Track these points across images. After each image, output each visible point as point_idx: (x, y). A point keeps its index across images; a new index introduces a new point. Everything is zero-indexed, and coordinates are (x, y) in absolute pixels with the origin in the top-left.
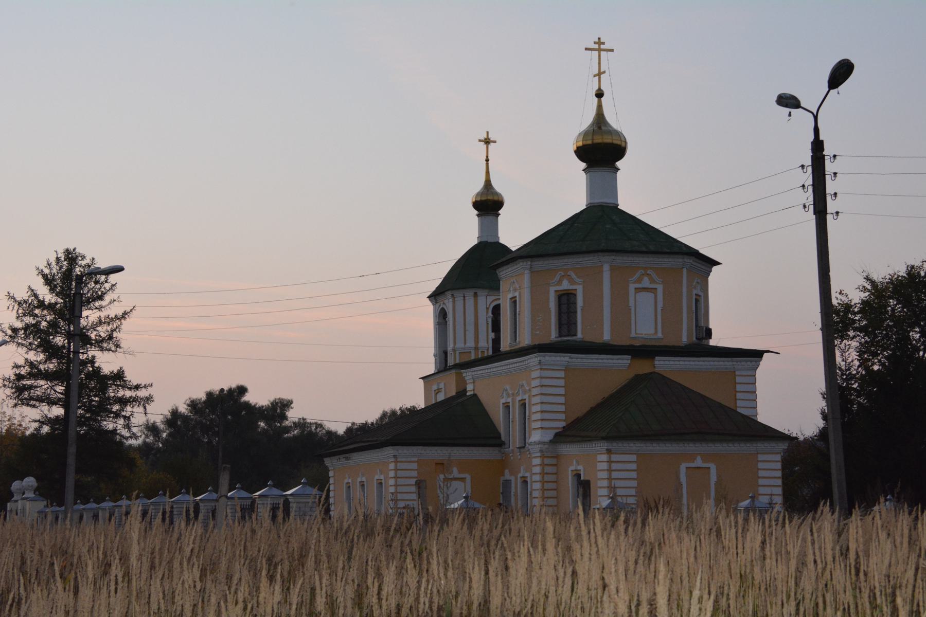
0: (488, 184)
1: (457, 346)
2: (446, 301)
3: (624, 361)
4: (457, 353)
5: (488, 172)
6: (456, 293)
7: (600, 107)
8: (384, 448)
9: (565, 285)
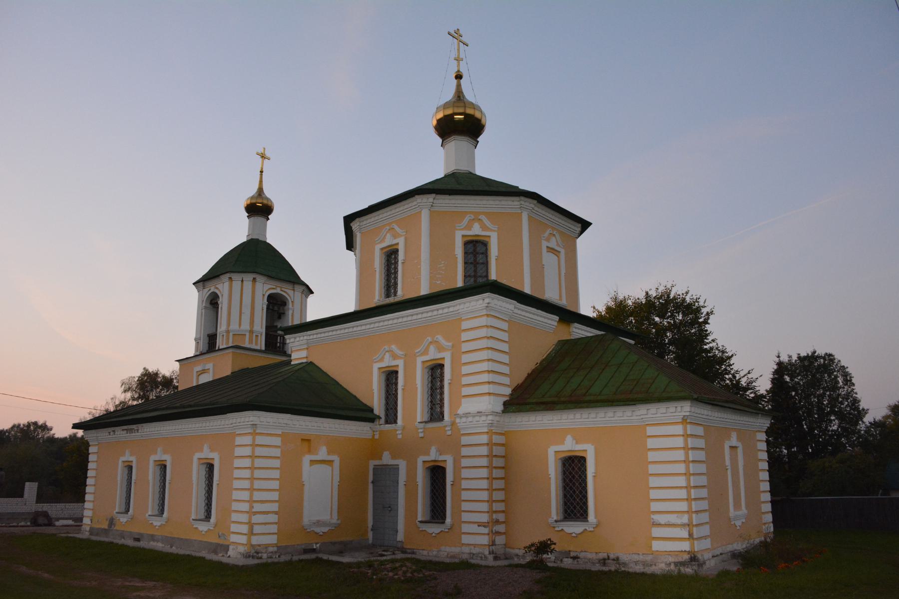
0: (260, 191)
1: (231, 328)
2: (220, 286)
3: (552, 320)
4: (231, 334)
5: (261, 182)
6: (235, 276)
7: (459, 86)
8: (229, 415)
9: (476, 230)
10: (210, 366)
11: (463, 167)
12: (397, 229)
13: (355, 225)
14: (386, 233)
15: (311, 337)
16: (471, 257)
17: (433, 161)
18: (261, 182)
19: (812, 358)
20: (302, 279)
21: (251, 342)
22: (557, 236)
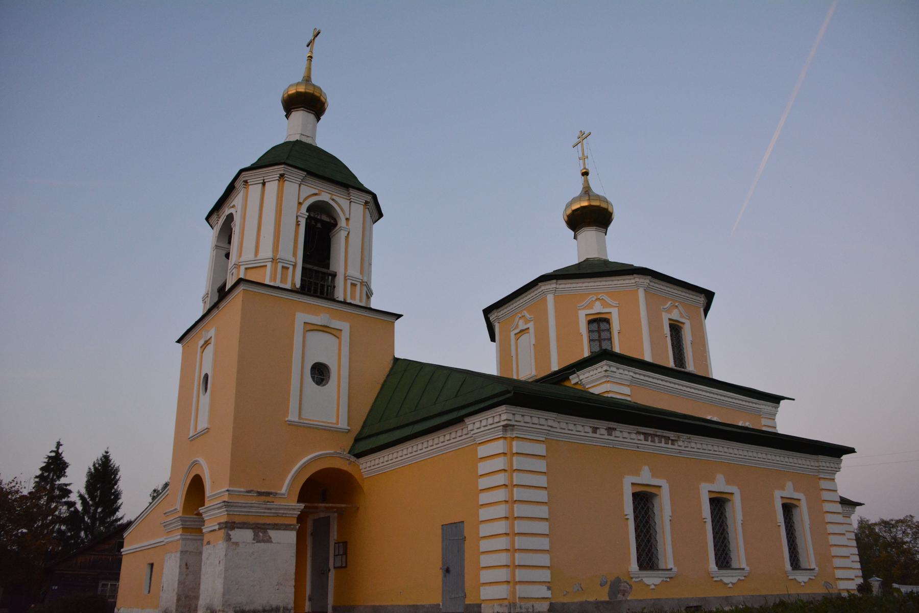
4: (349, 282)
5: (309, 69)
7: (586, 181)
9: (598, 308)
10: (212, 333)
11: (593, 254)
12: (528, 316)
13: (492, 317)
14: (519, 317)
15: (637, 376)
16: (604, 335)
17: (568, 250)
18: (309, 69)
21: (274, 278)
22: (680, 307)
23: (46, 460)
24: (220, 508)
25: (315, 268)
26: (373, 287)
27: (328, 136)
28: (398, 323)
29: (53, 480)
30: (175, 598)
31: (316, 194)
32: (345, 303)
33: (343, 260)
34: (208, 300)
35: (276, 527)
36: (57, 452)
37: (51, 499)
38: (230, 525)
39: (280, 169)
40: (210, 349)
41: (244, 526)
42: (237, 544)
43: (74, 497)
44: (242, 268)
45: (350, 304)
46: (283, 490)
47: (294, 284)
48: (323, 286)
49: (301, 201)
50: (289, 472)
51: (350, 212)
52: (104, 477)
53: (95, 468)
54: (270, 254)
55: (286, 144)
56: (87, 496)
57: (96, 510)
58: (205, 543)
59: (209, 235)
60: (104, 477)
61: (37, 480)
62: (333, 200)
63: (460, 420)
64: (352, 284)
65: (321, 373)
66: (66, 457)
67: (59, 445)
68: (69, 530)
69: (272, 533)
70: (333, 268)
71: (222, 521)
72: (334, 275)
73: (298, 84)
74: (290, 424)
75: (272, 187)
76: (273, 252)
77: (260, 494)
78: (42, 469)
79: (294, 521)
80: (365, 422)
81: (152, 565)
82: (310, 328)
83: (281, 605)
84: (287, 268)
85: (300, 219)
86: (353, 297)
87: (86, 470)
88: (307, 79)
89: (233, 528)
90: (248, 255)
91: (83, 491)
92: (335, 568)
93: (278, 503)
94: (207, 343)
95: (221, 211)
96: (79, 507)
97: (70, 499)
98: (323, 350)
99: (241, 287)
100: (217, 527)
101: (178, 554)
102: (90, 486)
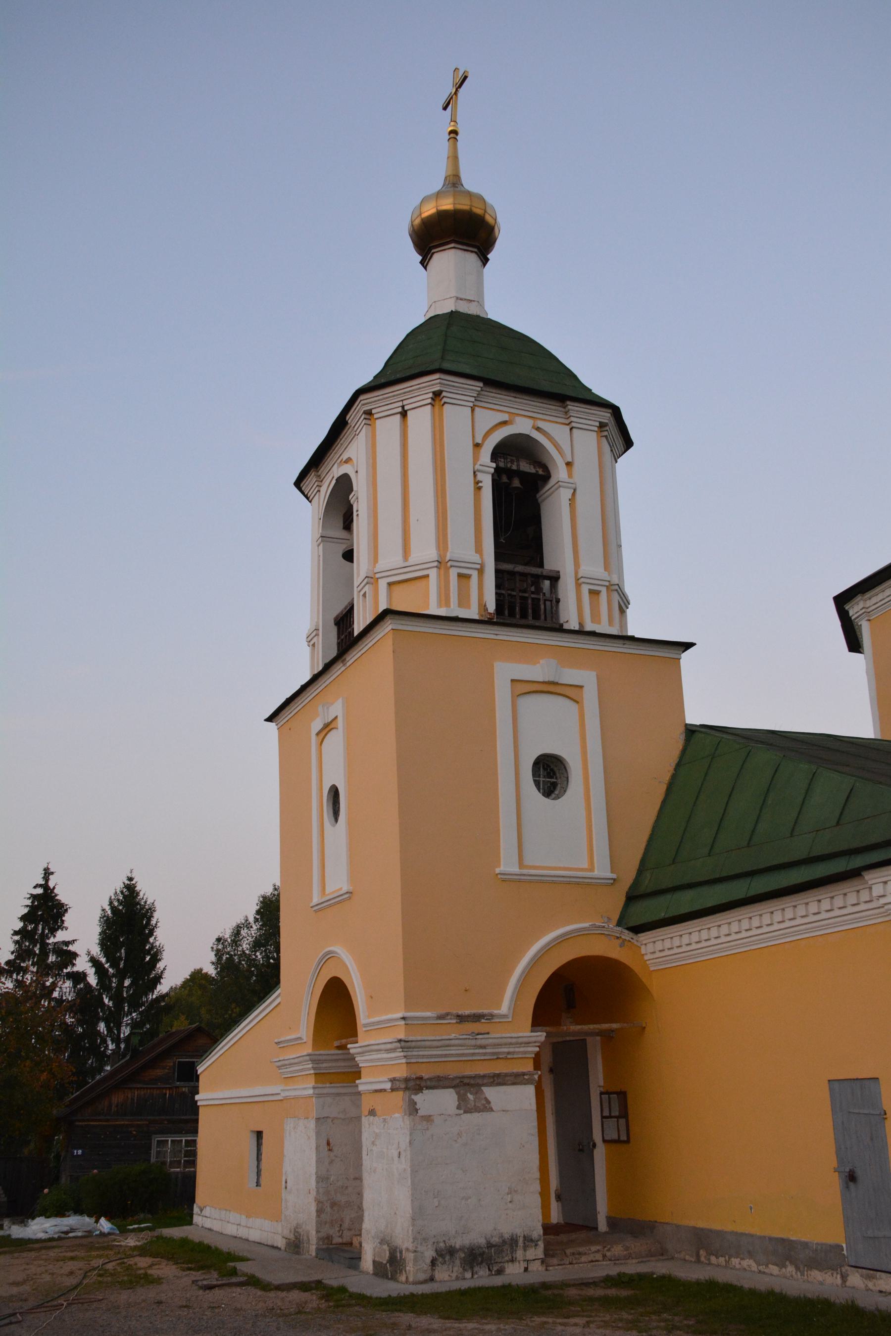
1: (383, 564)
4: (585, 589)
5: (454, 158)
10: (337, 709)
13: (854, 609)
18: (454, 158)
19: (277, 983)
20: (586, 379)
21: (444, 599)
23: (29, 902)
24: (393, 1050)
25: (520, 568)
26: (628, 590)
27: (510, 293)
28: (686, 657)
29: (44, 937)
30: (313, 1208)
31: (505, 423)
32: (581, 633)
33: (566, 546)
34: (319, 641)
35: (498, 1080)
36: (45, 887)
37: (45, 970)
38: (415, 1085)
39: (433, 382)
40: (335, 739)
41: (438, 1083)
42: (428, 1119)
43: (82, 965)
44: (383, 584)
45: (593, 634)
46: (504, 1008)
47: (483, 607)
48: (536, 602)
49: (479, 440)
50: (510, 972)
51: (567, 443)
52: (129, 922)
53: (113, 909)
54: (431, 554)
55: (432, 322)
56: (103, 960)
57: (120, 983)
58: (365, 1111)
59: (304, 516)
60: (129, 922)
61: (17, 938)
62: (538, 429)
63: (855, 874)
64: (591, 592)
65: (551, 773)
66: (62, 895)
67: (47, 873)
68: (80, 1022)
69: (491, 1093)
70: (550, 564)
71: (397, 1075)
72: (555, 578)
73: (438, 195)
74: (506, 880)
75: (421, 419)
76: (438, 548)
77: (462, 1019)
78: (23, 918)
79: (529, 1067)
80: (643, 862)
81: (259, 1134)
82: (524, 689)
83: (519, 1232)
84: (468, 577)
85: (480, 476)
86: (596, 618)
87: (98, 914)
88: (454, 182)
89: (419, 1089)
90: (391, 559)
91: (96, 951)
92: (604, 1141)
93: (497, 1034)
94: (328, 727)
95: (323, 469)
96: (93, 980)
97: (75, 969)
98: (551, 727)
99: (388, 626)
100: (388, 1086)
101: (312, 1124)
102: (108, 942)
